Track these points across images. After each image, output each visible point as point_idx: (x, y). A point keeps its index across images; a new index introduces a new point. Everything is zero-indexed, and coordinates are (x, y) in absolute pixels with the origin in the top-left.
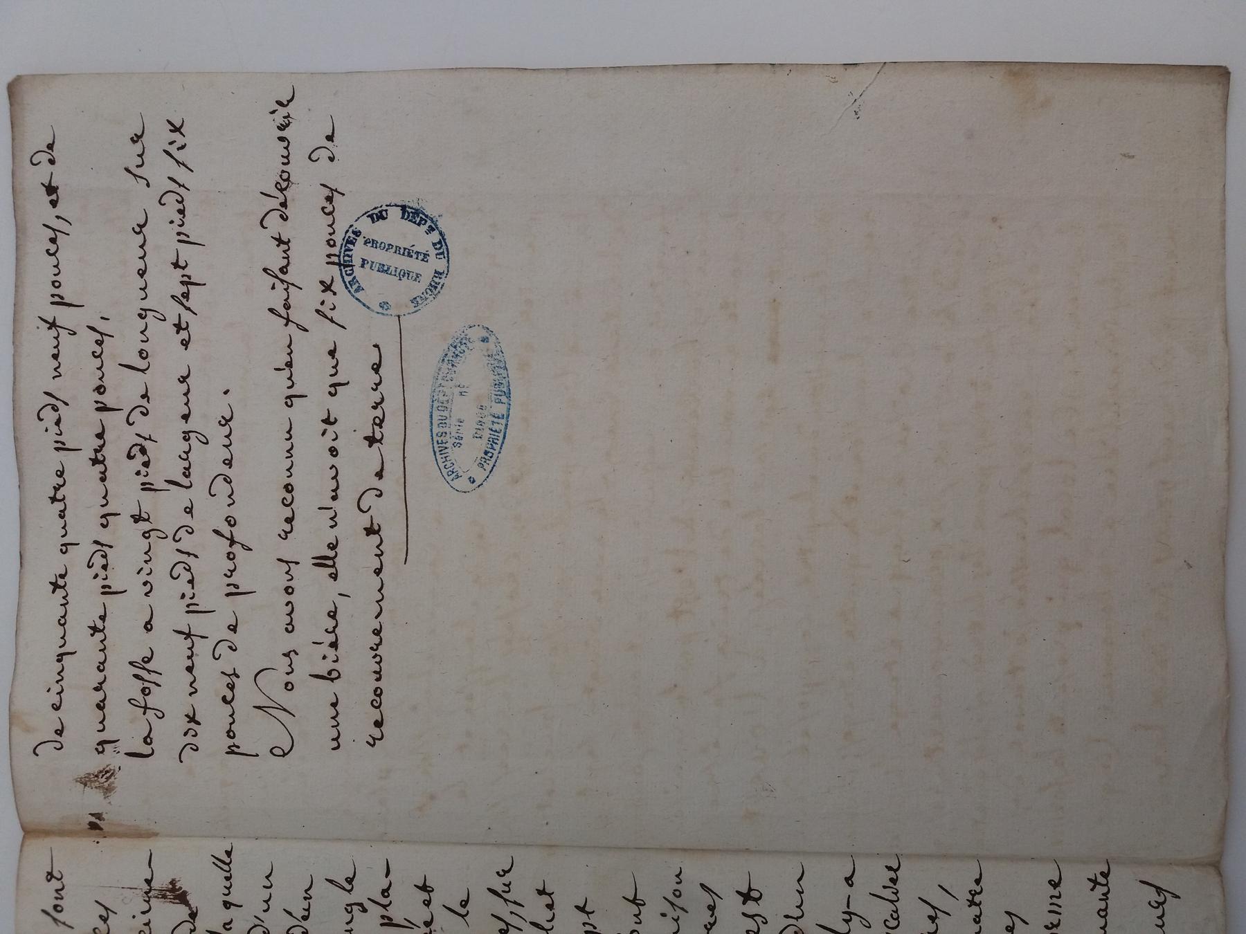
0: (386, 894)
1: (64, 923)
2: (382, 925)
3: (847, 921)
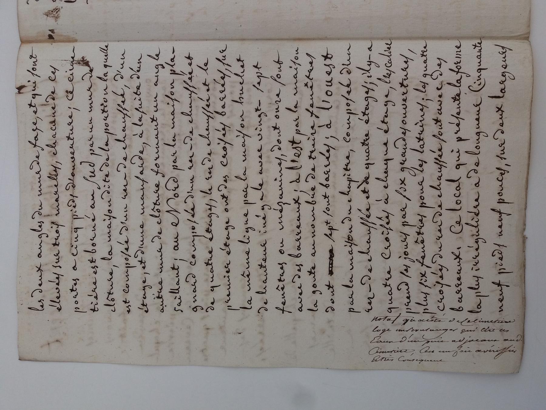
0: (173, 60)
1: (36, 75)
2: (171, 74)
3: (369, 65)
